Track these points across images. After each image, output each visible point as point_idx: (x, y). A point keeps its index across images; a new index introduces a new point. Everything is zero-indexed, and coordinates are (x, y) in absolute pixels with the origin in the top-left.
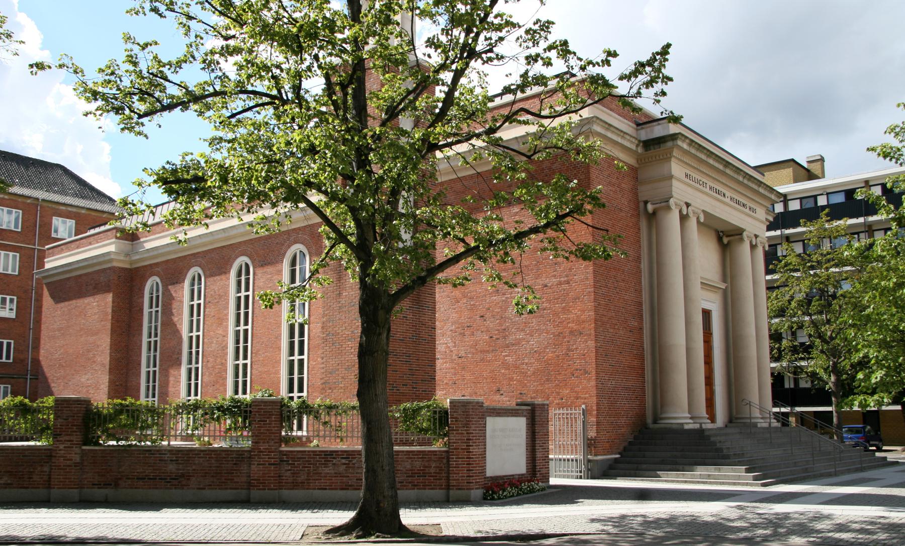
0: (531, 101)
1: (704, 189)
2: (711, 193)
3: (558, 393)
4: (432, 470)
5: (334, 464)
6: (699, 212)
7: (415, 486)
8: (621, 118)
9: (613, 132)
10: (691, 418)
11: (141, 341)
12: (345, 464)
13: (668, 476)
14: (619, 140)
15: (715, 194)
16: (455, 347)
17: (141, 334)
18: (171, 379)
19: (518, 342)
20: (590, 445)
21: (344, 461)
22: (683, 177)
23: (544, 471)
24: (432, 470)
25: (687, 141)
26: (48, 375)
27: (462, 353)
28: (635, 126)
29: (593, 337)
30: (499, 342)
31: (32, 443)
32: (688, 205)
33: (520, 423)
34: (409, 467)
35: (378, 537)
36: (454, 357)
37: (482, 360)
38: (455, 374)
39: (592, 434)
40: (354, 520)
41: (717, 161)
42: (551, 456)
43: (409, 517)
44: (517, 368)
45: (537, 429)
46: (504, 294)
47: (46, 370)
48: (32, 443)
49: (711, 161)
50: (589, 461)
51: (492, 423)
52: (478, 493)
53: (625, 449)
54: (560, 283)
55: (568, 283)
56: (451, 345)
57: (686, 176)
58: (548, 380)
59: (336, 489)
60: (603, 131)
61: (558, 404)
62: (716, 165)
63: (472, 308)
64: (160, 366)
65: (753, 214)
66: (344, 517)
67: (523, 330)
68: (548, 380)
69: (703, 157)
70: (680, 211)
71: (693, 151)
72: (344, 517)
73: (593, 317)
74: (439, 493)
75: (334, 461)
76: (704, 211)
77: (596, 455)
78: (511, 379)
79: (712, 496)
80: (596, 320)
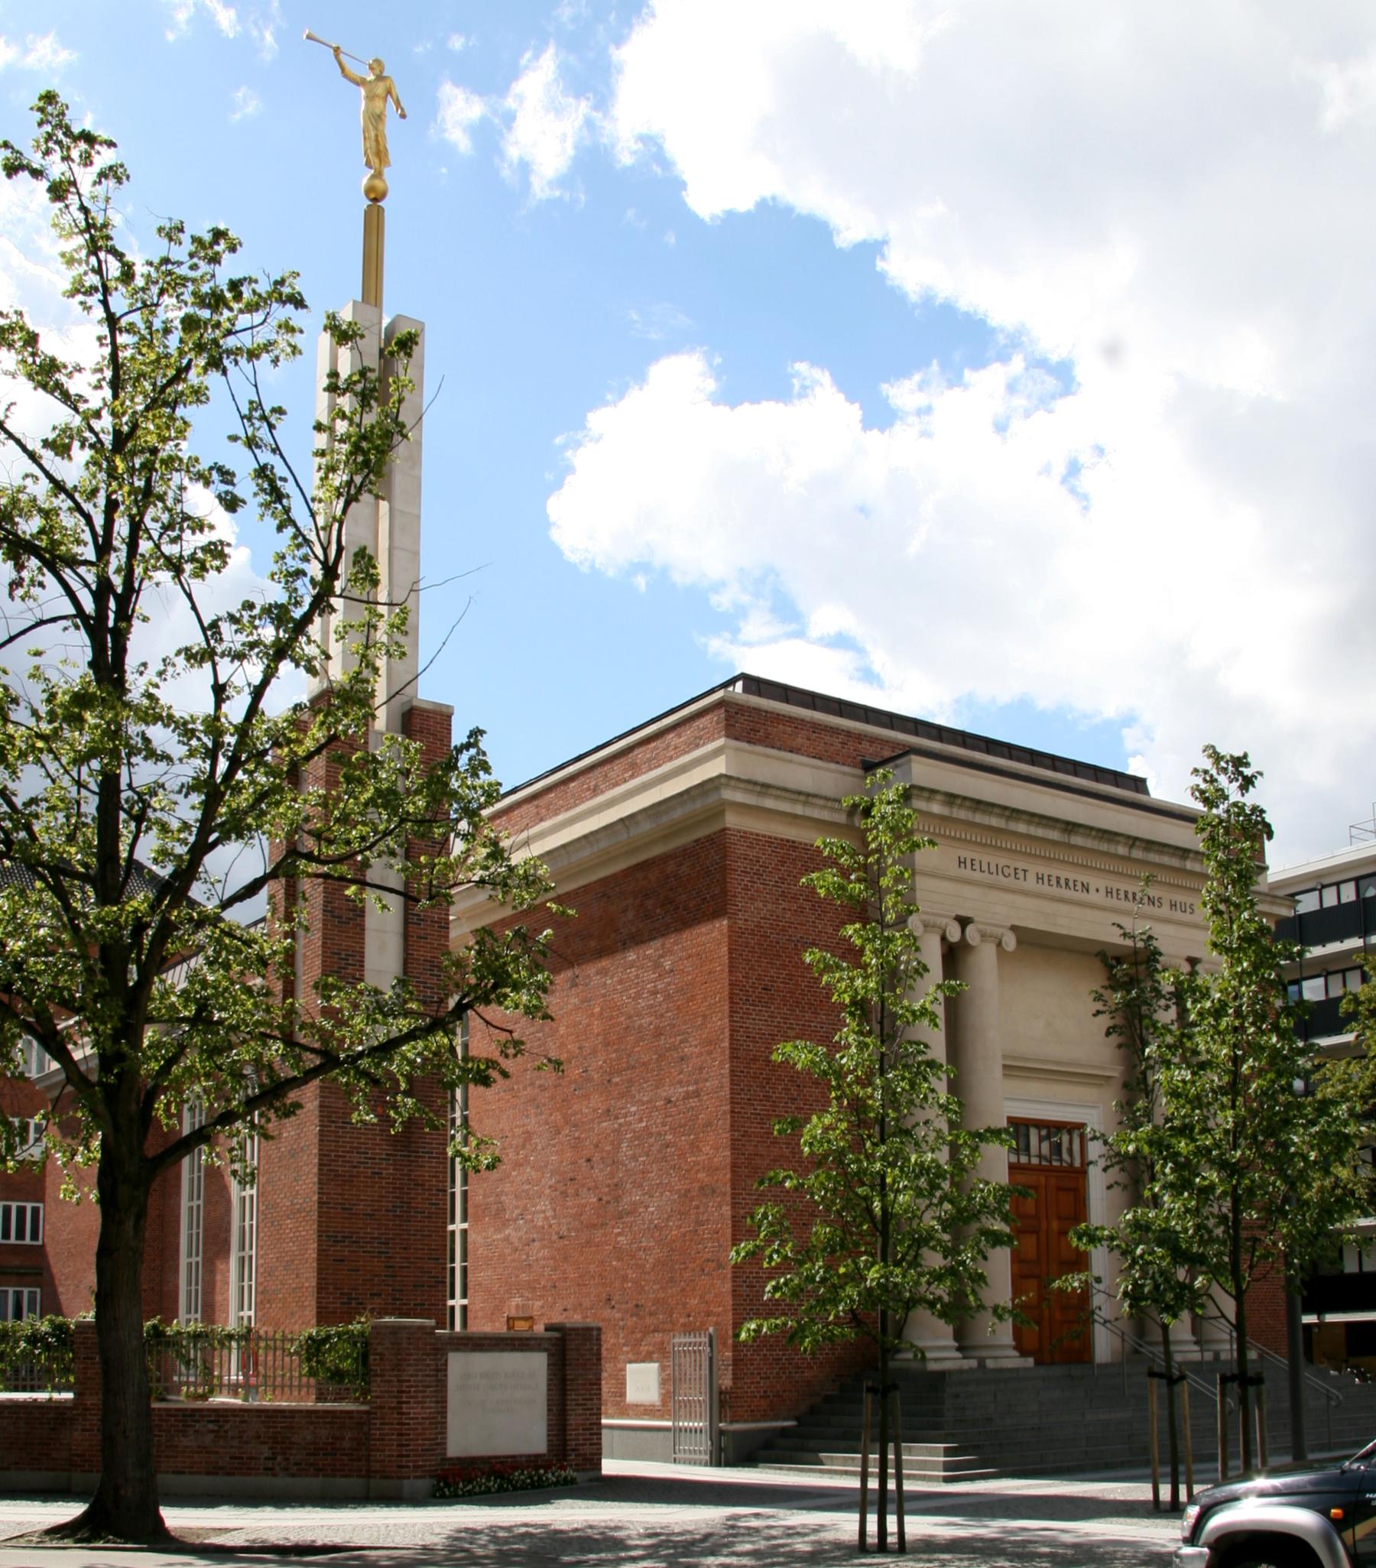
0: (653, 745)
1: (1021, 884)
2: (1045, 889)
3: (684, 1305)
4: (346, 1444)
5: (196, 1431)
6: (999, 931)
7: (319, 1471)
8: (819, 763)
9: (777, 797)
10: (1196, 1343)
11: (179, 1206)
12: (213, 1431)
13: (832, 1462)
14: (799, 810)
15: (1054, 890)
16: (554, 1217)
17: (178, 1194)
18: (219, 1277)
19: (635, 1206)
20: (723, 1403)
21: (211, 1426)
22: (954, 870)
23: (587, 1449)
24: (346, 1444)
25: (939, 797)
26: (55, 1271)
27: (564, 1231)
28: (860, 772)
29: (728, 1199)
30: (610, 1207)
31: (42, 1396)
32: (964, 922)
33: (537, 1363)
34: (309, 1438)
35: (108, 1542)
36: (555, 1237)
37: (588, 1243)
38: (555, 1269)
39: (727, 1382)
40: (85, 1514)
41: (1045, 826)
42: (604, 1421)
43: (174, 1518)
44: (633, 1257)
45: (570, 1373)
46: (617, 1118)
47: (52, 1261)
48: (42, 1396)
49: (1021, 828)
50: (722, 1432)
51: (457, 1363)
52: (424, 1484)
53: (812, 1411)
54: (687, 1096)
55: (698, 1096)
56: (549, 1213)
57: (962, 862)
58: (671, 1280)
59: (200, 1473)
60: (750, 800)
61: (684, 1325)
62: (1040, 832)
63: (577, 1145)
64: (204, 1253)
65: (1186, 917)
66: (70, 1511)
67: (640, 1186)
68: (671, 1280)
69: (995, 822)
70: (944, 939)
71: (962, 814)
72: (70, 1511)
73: (729, 1160)
74: (354, 1483)
75: (197, 1426)
76: (1014, 928)
77: (732, 1422)
78: (625, 1278)
79: (940, 1498)
80: (734, 1166)
